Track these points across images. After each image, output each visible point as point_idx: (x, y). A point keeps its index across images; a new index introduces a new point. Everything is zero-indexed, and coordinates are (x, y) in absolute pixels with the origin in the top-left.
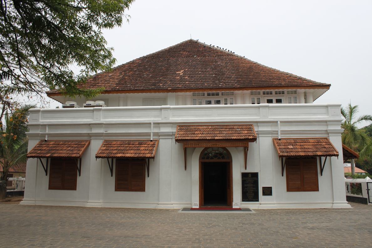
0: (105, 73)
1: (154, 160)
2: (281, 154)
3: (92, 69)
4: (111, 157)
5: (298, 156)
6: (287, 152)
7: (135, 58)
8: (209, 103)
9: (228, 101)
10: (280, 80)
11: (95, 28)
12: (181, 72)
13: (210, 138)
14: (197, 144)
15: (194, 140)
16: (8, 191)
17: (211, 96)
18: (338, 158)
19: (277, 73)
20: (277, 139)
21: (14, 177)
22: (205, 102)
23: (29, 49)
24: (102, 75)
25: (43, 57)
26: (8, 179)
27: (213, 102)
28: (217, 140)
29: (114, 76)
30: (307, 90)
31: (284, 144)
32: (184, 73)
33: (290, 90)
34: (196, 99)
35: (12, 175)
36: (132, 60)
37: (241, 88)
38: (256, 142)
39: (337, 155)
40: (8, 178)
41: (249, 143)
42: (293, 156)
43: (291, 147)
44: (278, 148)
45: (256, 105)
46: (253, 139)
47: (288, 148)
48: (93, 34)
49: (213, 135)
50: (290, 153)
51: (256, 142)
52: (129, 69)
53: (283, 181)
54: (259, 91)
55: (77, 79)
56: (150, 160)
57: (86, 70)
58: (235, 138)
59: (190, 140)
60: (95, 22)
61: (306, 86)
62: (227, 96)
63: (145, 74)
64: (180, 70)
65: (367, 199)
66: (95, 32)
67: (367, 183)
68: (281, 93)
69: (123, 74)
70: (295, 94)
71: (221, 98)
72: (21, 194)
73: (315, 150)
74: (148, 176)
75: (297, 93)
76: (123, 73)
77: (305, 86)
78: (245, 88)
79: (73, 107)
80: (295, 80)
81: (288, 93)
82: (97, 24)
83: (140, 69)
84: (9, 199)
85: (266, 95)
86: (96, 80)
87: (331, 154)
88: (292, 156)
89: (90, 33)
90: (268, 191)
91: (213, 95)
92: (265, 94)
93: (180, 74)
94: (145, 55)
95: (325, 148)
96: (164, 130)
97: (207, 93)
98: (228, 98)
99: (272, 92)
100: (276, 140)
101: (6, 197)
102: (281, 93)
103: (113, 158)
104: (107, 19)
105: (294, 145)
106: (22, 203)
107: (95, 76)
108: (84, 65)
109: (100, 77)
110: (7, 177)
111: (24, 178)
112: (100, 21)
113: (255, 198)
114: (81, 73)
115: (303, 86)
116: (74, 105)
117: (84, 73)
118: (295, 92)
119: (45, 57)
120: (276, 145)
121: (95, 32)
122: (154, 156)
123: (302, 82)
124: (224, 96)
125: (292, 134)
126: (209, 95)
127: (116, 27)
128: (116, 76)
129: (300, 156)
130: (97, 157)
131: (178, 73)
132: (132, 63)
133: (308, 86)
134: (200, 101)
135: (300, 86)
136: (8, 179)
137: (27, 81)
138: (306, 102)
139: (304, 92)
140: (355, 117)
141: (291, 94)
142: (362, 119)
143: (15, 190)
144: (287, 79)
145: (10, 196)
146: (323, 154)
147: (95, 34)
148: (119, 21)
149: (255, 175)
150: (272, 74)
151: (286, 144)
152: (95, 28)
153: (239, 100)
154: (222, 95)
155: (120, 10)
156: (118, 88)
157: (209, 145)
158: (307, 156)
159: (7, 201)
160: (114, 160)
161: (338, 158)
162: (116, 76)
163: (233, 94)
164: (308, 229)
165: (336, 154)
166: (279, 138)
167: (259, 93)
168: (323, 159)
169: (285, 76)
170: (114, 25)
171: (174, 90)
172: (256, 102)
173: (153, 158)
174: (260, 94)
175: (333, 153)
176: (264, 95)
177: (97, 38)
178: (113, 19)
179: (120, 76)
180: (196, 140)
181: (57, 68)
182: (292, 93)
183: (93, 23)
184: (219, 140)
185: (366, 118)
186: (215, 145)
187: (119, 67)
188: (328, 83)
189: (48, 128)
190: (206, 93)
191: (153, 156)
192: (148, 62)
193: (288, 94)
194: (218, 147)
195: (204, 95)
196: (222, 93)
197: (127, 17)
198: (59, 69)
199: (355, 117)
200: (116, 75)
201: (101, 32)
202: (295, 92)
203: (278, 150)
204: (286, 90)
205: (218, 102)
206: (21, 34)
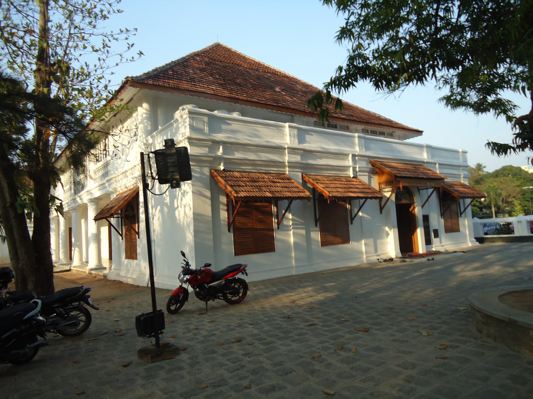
125: (454, 177)
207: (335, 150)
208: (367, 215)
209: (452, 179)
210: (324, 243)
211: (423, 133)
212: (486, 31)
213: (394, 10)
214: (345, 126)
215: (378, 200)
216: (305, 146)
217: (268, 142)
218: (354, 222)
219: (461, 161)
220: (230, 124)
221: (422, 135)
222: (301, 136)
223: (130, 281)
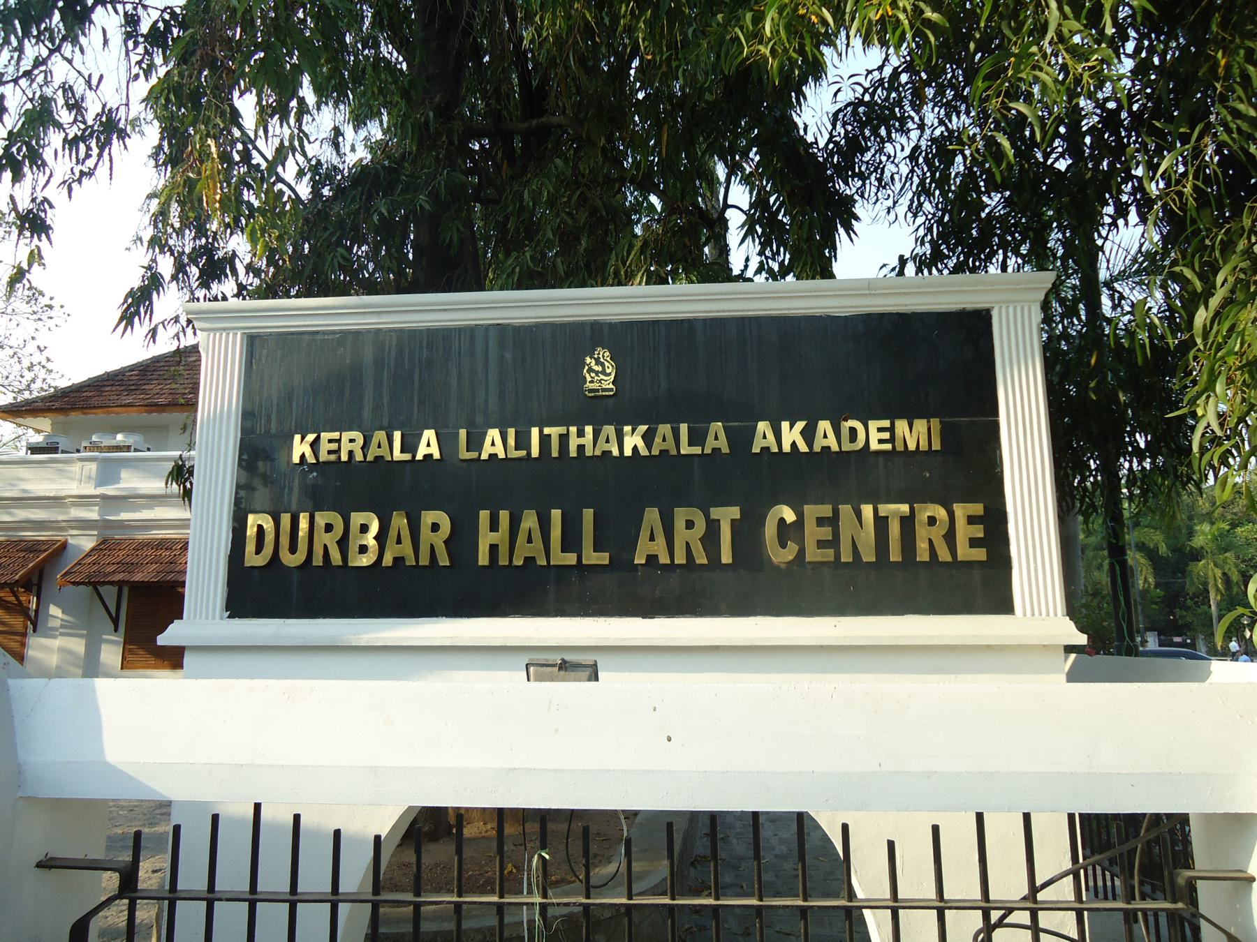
116: (58, 443)
160: (126, 591)
216: (109, 490)
217: (25, 491)
222: (107, 474)
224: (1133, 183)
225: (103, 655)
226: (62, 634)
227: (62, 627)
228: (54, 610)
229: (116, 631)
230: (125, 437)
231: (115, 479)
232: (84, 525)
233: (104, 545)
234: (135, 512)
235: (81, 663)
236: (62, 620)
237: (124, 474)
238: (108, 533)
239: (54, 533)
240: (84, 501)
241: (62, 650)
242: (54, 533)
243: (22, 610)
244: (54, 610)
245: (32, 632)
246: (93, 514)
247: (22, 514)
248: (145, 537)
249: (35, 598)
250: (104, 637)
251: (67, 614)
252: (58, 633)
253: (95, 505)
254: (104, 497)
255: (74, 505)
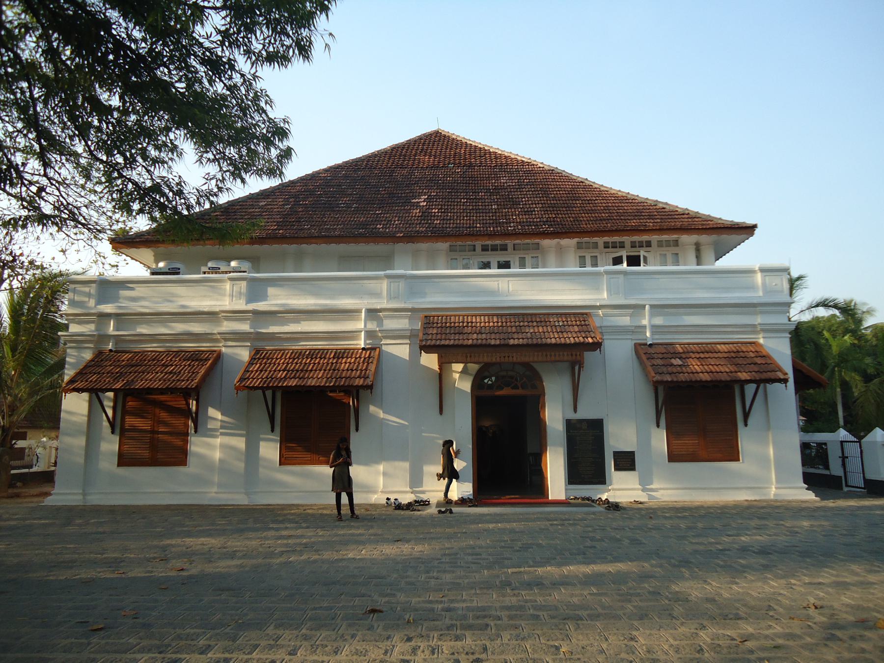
0: (250, 199)
1: (371, 392)
2: (658, 378)
3: (233, 174)
4: (268, 388)
5: (696, 381)
6: (670, 374)
7: (316, 169)
8: (486, 265)
9: (528, 261)
10: (642, 217)
11: (243, 64)
12: (420, 200)
13: (498, 342)
14: (469, 355)
15: (462, 346)
16: (13, 472)
17: (490, 252)
18: (786, 386)
19: (634, 201)
20: (645, 344)
21: (29, 439)
22: (476, 264)
23: (66, 120)
24: (244, 204)
25: (105, 142)
26: (15, 443)
27: (494, 263)
28: (513, 346)
29: (270, 207)
30: (704, 238)
31: (660, 356)
32: (429, 200)
33: (665, 237)
34: (456, 259)
35: (25, 433)
36: (310, 172)
37: (558, 233)
38: (600, 351)
39: (785, 381)
40: (14, 442)
41: (585, 353)
42: (686, 382)
43: (679, 362)
44: (650, 364)
45: (589, 269)
46: (593, 343)
47: (672, 365)
48: (237, 79)
49: (505, 336)
50: (676, 377)
51: (600, 351)
52: (304, 192)
53: (660, 440)
54: (596, 239)
55: (195, 198)
56: (361, 391)
57: (219, 176)
58: (516, 342)
59: (453, 346)
60: (242, 49)
61: (702, 229)
62: (526, 252)
63: (341, 204)
64: (419, 197)
65: (841, 477)
66: (243, 75)
67: (842, 442)
68: (645, 245)
69: (291, 202)
70: (674, 246)
71: (512, 256)
72: (48, 478)
73: (732, 368)
74: (357, 430)
75: (679, 244)
76: (291, 200)
77: (698, 228)
78: (566, 233)
79: (178, 273)
80: (676, 217)
81: (660, 244)
82: (248, 52)
83: (330, 191)
84: (16, 491)
85: (610, 250)
86: (229, 215)
87: (773, 377)
88: (682, 381)
89: (231, 78)
90: (626, 461)
91: (494, 248)
92: (608, 247)
93: (422, 204)
94: (339, 161)
95: (755, 364)
96: (391, 324)
97: (482, 245)
98: (526, 256)
99: (624, 242)
100: (642, 346)
101: (11, 486)
102: (645, 245)
103: (275, 389)
104: (273, 41)
105: (684, 358)
106: (49, 501)
107: (227, 205)
108: (213, 161)
109: (238, 207)
110: (12, 439)
111: (55, 441)
112: (257, 46)
113: (599, 478)
114: (205, 181)
115: (694, 229)
116: (179, 269)
117: (214, 182)
118: (676, 243)
119: (109, 142)
120: (644, 357)
121: (243, 75)
122: (372, 384)
123: (690, 220)
124: (518, 252)
125: (702, 333)
126: (485, 249)
127: (297, 64)
128: (277, 207)
129: (701, 381)
130: (237, 389)
131: (414, 201)
132: (310, 180)
133: (706, 228)
134: (465, 262)
135: (688, 229)
136: (15, 443)
137: (65, 203)
138: (698, 264)
139: (695, 241)
140: (802, 299)
141: (646, 247)
142: (817, 306)
143: (31, 470)
144: (656, 213)
145: (19, 484)
146: (753, 378)
147: (242, 80)
148: (304, 50)
149: (597, 426)
150: (623, 205)
151: (665, 355)
152: (243, 64)
153: (552, 258)
154: (514, 249)
155: (305, 20)
156: (281, 231)
157: (495, 358)
158: (716, 381)
159: (12, 497)
160: (279, 395)
161: (786, 386)
162: (277, 207)
163: (537, 247)
164: (754, 552)
165: (782, 377)
166: (648, 343)
167: (595, 246)
168: (750, 389)
169: (651, 208)
170: (293, 59)
171: (411, 238)
172: (588, 261)
173: (370, 387)
174: (597, 248)
175: (776, 374)
176: (607, 250)
177: (247, 91)
178: (288, 42)
179: (286, 207)
180: (467, 346)
181: (143, 169)
182: (668, 244)
183: (236, 51)
184: (518, 345)
185: (826, 303)
186: (509, 357)
187: (280, 187)
188: (750, 221)
189: (380, 407)
190: (479, 244)
191: (370, 383)
192: (346, 177)
193: (658, 246)
194: (514, 363)
195: (474, 250)
196: (514, 245)
197: (327, 37)
198: (148, 171)
199: (802, 299)
200: (275, 203)
201: (257, 77)
202: (676, 243)
203: (650, 369)
204: (654, 238)
205: (506, 265)
206: (45, 81)
207: (315, 305)
208: (397, 417)
209: (719, 336)
210: (124, 460)
211: (757, 231)
212: (99, 54)
213: (93, 78)
214: (523, 250)
215: (260, 392)
216: (261, 306)
217: (183, 306)
218: (750, 422)
219: (761, 294)
220: (132, 289)
221: (752, 234)
222: (256, 290)
223: (466, 483)
224: (51, 220)
225: (261, 450)
226: (222, 434)
227: (222, 427)
228: (213, 412)
229: (273, 431)
230: (239, 264)
231: (263, 297)
232: (239, 337)
233: (257, 355)
234: (283, 325)
235: (243, 457)
236: (221, 421)
237: (271, 291)
238: (260, 344)
239: (211, 345)
240: (236, 315)
241: (223, 446)
242: (211, 345)
243: (187, 413)
244: (213, 412)
245: (193, 432)
246: (245, 327)
247: (180, 327)
248: (297, 347)
249: (195, 402)
250: (262, 436)
251: (226, 416)
252: (219, 433)
253: (248, 319)
254: (256, 313)
255: (227, 319)
